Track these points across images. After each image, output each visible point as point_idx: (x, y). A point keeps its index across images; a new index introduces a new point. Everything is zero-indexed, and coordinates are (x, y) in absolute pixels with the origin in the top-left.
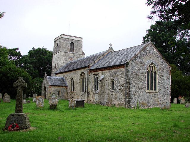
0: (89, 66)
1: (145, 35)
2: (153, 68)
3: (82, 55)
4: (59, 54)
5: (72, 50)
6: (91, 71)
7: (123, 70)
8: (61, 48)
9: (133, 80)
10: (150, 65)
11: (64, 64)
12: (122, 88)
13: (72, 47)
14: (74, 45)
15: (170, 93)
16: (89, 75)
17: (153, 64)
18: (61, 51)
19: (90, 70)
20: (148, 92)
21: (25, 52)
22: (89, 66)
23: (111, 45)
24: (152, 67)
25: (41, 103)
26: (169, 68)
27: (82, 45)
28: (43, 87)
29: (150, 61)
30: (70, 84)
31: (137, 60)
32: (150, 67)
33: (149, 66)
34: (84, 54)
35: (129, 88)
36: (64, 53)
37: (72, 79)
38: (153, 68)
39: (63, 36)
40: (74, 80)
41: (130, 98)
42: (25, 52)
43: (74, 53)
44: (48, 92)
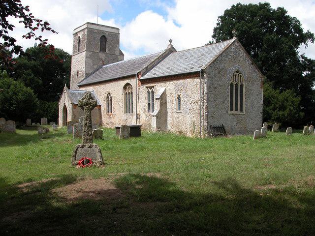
5: (103, 49)
6: (143, 82)
10: (235, 74)
12: (194, 107)
15: (261, 115)
19: (140, 80)
21: (248, 5)
23: (171, 41)
24: (237, 77)
30: (106, 102)
32: (235, 76)
33: (233, 76)
37: (109, 94)
42: (248, 5)
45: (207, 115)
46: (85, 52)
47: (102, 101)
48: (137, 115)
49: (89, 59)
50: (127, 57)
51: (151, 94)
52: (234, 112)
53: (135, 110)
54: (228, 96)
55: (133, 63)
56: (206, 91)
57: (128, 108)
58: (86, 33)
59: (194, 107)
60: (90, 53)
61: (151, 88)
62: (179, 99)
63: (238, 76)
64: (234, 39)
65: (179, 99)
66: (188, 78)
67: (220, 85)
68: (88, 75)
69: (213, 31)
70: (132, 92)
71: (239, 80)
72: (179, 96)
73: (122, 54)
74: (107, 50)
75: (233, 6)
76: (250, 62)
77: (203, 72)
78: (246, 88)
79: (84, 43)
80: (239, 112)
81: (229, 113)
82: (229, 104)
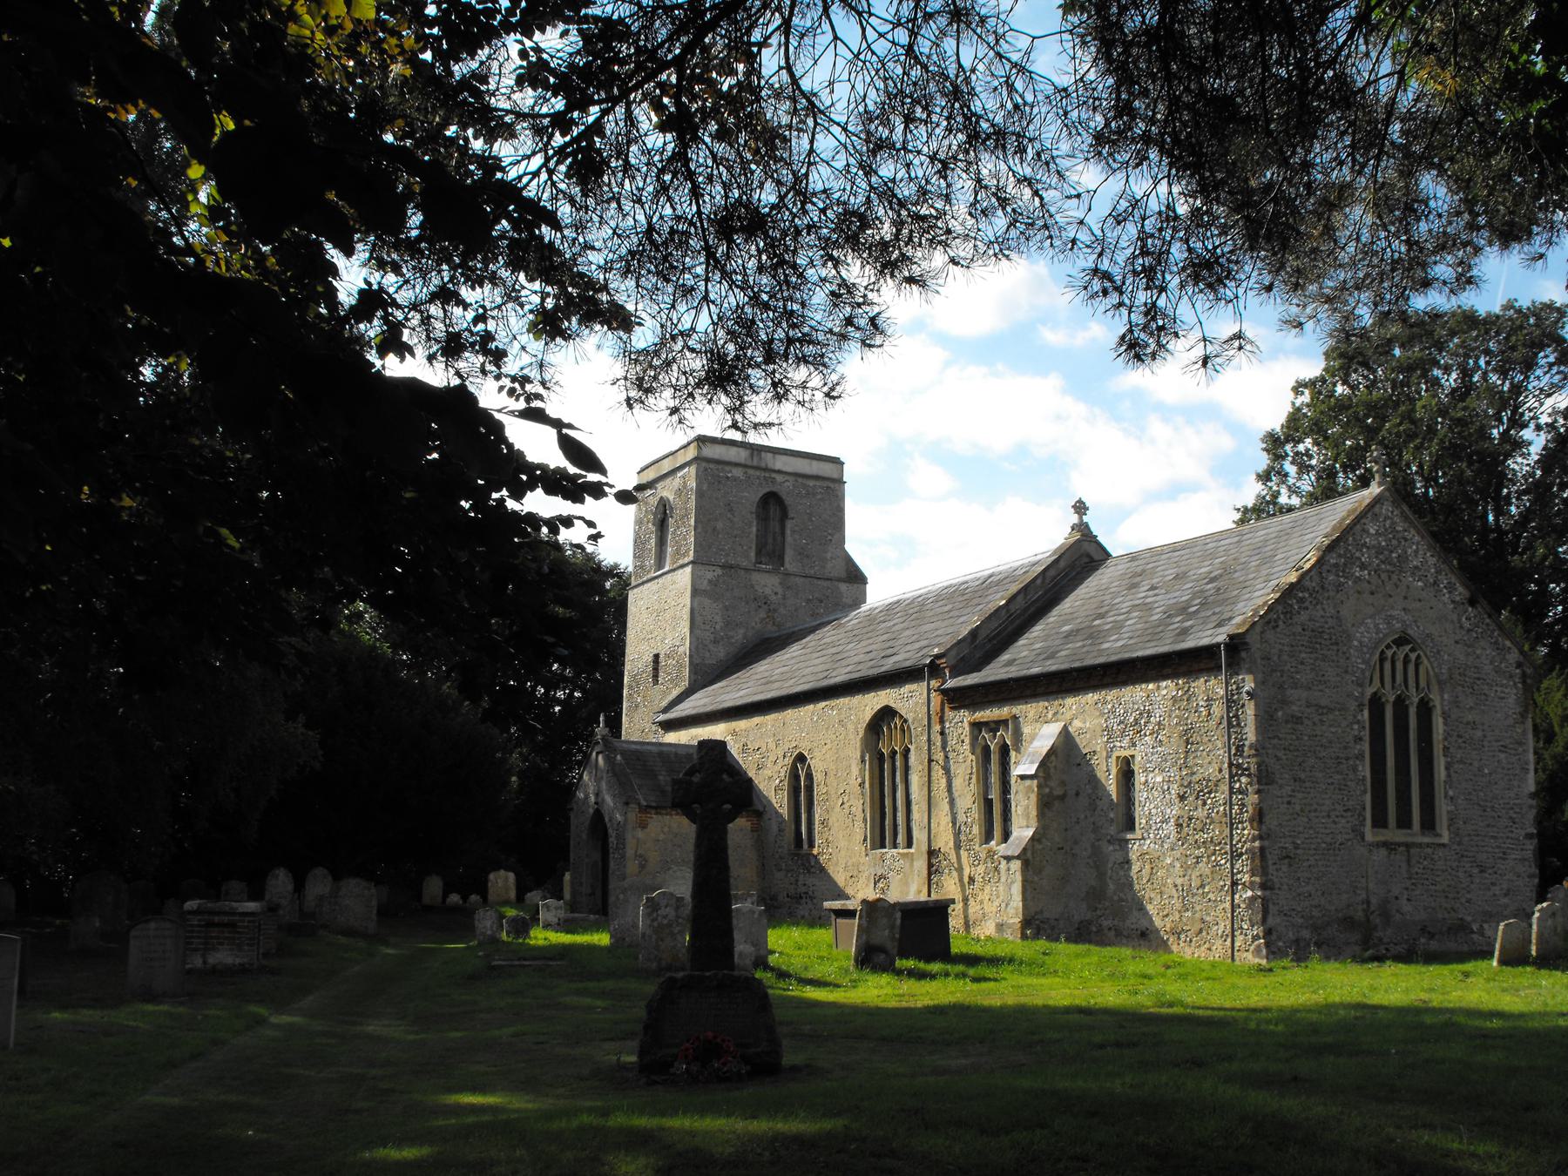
1: (1275, 421)
2: (1411, 667)
3: (843, 587)
5: (770, 552)
6: (958, 699)
9: (1280, 754)
10: (1389, 653)
13: (774, 525)
14: (784, 515)
15: (1531, 846)
17: (1408, 642)
19: (944, 692)
20: (1385, 844)
23: (1080, 508)
24: (1399, 666)
25: (670, 925)
26: (1519, 665)
28: (579, 826)
29: (1389, 620)
31: (1304, 616)
32: (1388, 666)
33: (1382, 659)
36: (719, 571)
37: (801, 758)
38: (1411, 667)
40: (817, 764)
43: (790, 564)
44: (630, 852)
45: (1262, 849)
46: (688, 569)
47: (770, 783)
48: (931, 853)
49: (707, 602)
50: (878, 593)
51: (994, 758)
52: (1393, 834)
53: (919, 835)
54: (1360, 756)
55: (913, 610)
56: (1251, 735)
57: (886, 828)
58: (693, 484)
60: (710, 574)
63: (1406, 661)
64: (1375, 489)
67: (1319, 706)
68: (704, 674)
69: (1546, 299)
70: (907, 751)
71: (1388, 679)
73: (856, 578)
74: (787, 559)
76: (1461, 592)
77: (1236, 645)
78: (631, 687)
79: (684, 534)
80: (1415, 834)
81: (1369, 837)
82: (1368, 798)
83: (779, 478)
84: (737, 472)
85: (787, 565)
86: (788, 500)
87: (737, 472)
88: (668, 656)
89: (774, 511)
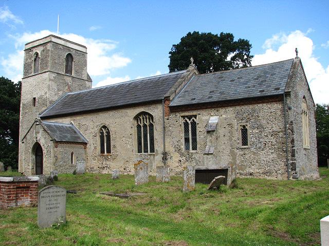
0: (167, 99)
3: (87, 82)
4: (46, 75)
5: (68, 70)
6: (174, 109)
7: (276, 107)
8: (49, 64)
11: (56, 98)
12: (274, 141)
13: (70, 63)
16: (166, 118)
18: (49, 69)
21: (200, 33)
22: (167, 99)
27: (86, 60)
30: (98, 139)
34: (89, 80)
35: (293, 141)
37: (104, 127)
39: (54, 40)
41: (295, 160)
42: (200, 33)
49: (53, 83)
53: (158, 147)
59: (274, 141)
61: (190, 117)
62: (244, 131)
65: (244, 131)
66: (231, 106)
72: (244, 127)
75: (190, 33)
83: (71, 50)
84: (61, 47)
85: (73, 74)
86: (74, 56)
87: (61, 47)
88: (39, 98)
89: (70, 59)
